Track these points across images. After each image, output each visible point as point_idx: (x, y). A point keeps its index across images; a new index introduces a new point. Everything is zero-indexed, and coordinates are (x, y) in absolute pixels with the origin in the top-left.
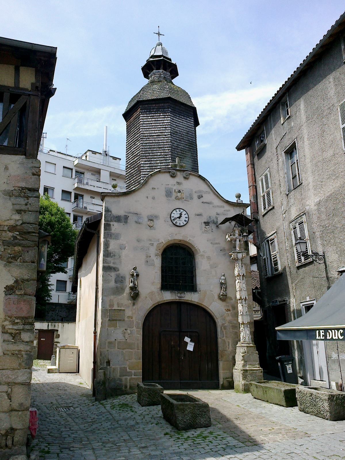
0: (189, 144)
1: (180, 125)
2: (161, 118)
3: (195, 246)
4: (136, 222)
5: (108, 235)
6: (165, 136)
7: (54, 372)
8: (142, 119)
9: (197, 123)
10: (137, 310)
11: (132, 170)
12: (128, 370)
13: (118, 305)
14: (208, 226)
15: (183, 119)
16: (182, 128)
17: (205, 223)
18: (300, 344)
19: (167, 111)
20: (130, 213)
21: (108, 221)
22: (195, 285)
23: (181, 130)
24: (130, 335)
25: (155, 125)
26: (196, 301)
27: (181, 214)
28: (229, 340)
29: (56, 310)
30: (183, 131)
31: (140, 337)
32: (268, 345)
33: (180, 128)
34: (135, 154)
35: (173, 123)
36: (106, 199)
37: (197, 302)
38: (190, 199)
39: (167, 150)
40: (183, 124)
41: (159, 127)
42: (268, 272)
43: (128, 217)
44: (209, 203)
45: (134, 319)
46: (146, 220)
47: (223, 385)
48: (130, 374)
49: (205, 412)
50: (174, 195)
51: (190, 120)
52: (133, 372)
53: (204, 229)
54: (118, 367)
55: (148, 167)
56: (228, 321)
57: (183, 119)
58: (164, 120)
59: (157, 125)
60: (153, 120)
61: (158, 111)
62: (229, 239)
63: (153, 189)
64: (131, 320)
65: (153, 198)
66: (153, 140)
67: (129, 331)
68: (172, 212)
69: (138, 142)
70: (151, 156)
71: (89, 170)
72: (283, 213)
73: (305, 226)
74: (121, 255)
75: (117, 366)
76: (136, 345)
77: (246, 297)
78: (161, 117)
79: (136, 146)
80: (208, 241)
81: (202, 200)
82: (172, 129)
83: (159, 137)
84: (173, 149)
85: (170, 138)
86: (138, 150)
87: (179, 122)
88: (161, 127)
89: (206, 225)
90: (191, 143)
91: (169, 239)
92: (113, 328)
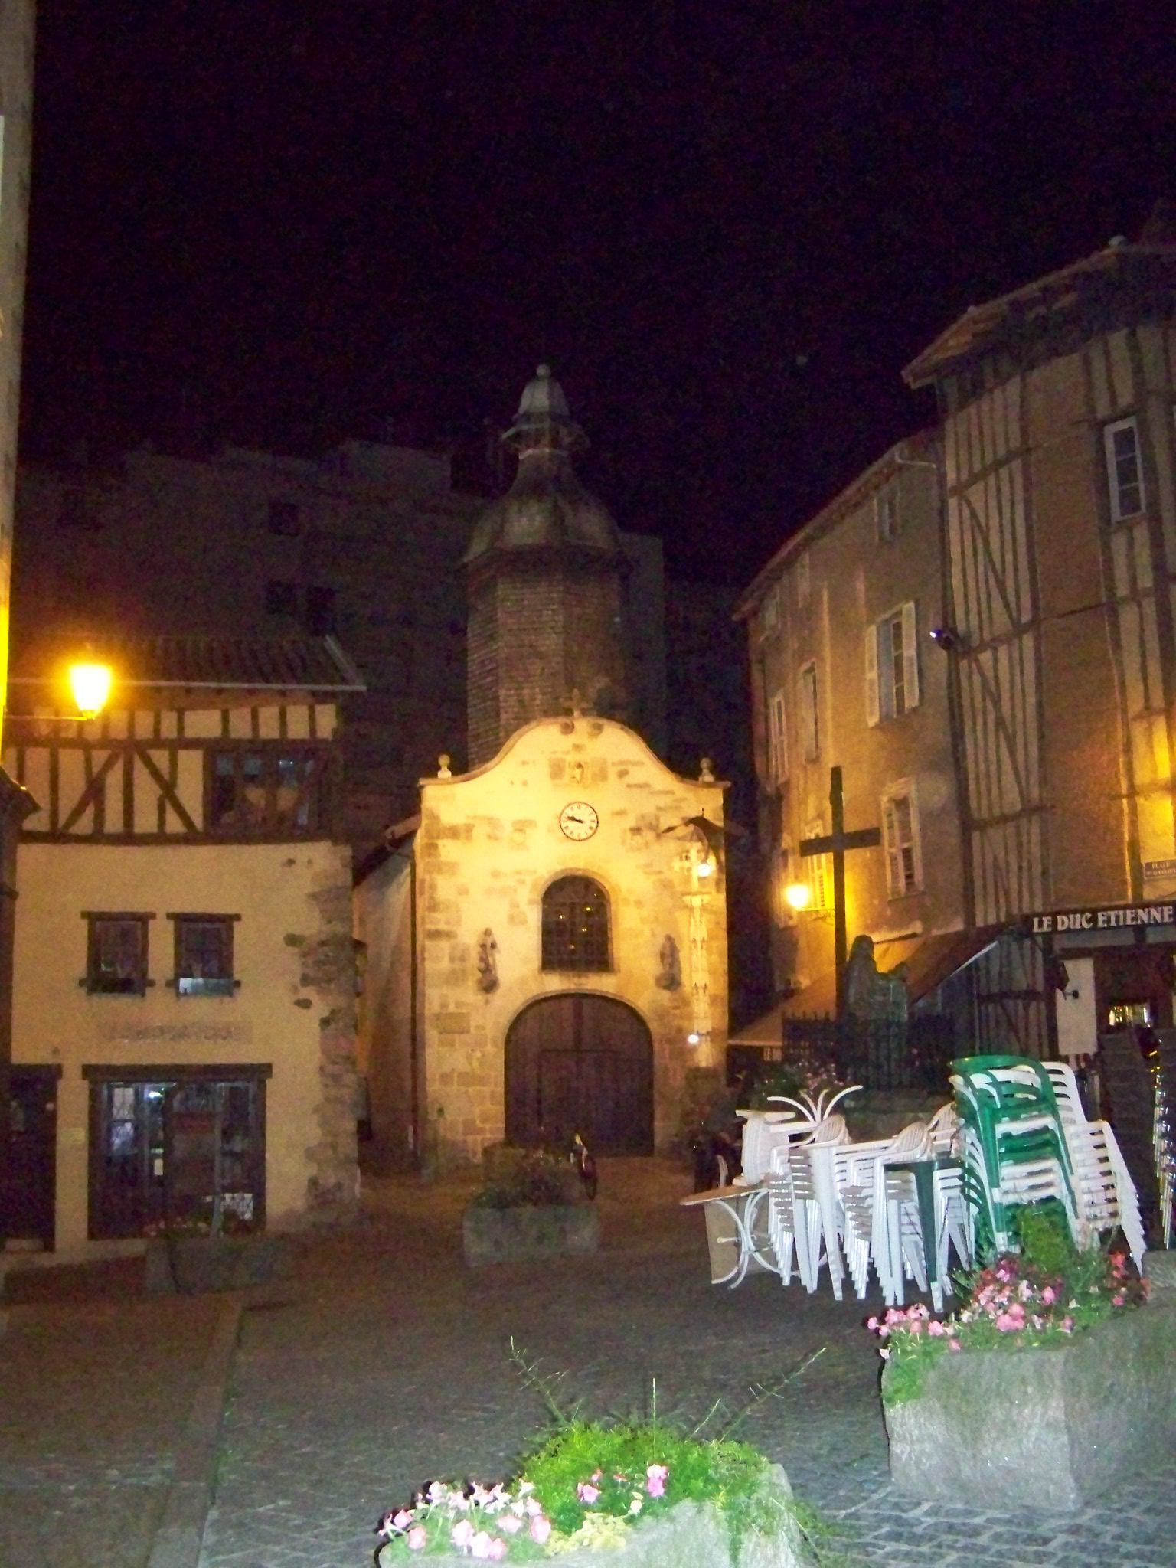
20: (475, 817)
46: (509, 828)
48: (481, 1131)
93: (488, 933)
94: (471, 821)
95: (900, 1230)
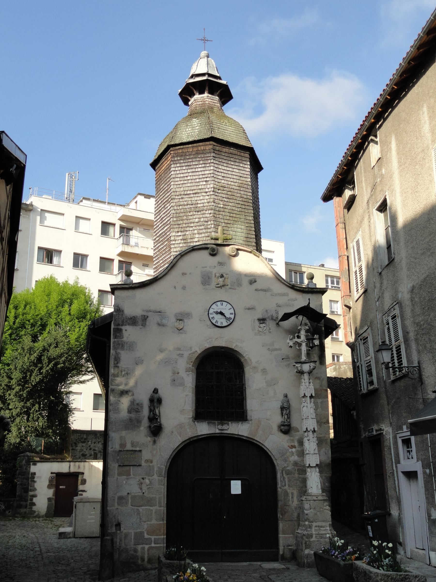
0: (242, 203)
1: (228, 176)
3: (244, 355)
4: (159, 324)
5: (119, 344)
7: (68, 536)
8: (174, 171)
10: (158, 450)
11: (160, 245)
12: (146, 536)
13: (133, 444)
14: (264, 325)
15: (233, 167)
17: (259, 320)
18: (398, 494)
20: (150, 311)
22: (245, 411)
24: (149, 486)
27: (217, 313)
28: (293, 491)
29: (88, 442)
30: (232, 183)
31: (163, 489)
32: (365, 493)
33: (229, 179)
34: (164, 222)
37: (246, 437)
38: (238, 286)
40: (234, 173)
42: (362, 387)
43: (148, 317)
45: (154, 463)
46: (172, 319)
47: (283, 555)
48: (149, 541)
50: (214, 281)
51: (244, 166)
52: (153, 539)
53: (257, 328)
54: (132, 532)
56: (292, 462)
60: (189, 171)
63: (184, 274)
64: (151, 464)
65: (184, 288)
67: (147, 481)
69: (169, 204)
70: (186, 224)
72: (376, 300)
73: (399, 321)
75: (130, 531)
76: (157, 500)
79: (166, 210)
80: (263, 346)
81: (255, 286)
82: (217, 183)
83: (197, 195)
84: (217, 212)
85: (212, 197)
86: (168, 215)
87: (227, 172)
89: (261, 323)
90: (245, 200)
91: (205, 347)
92: (126, 477)
93: (156, 391)
94: (145, 314)
95: (223, 232)
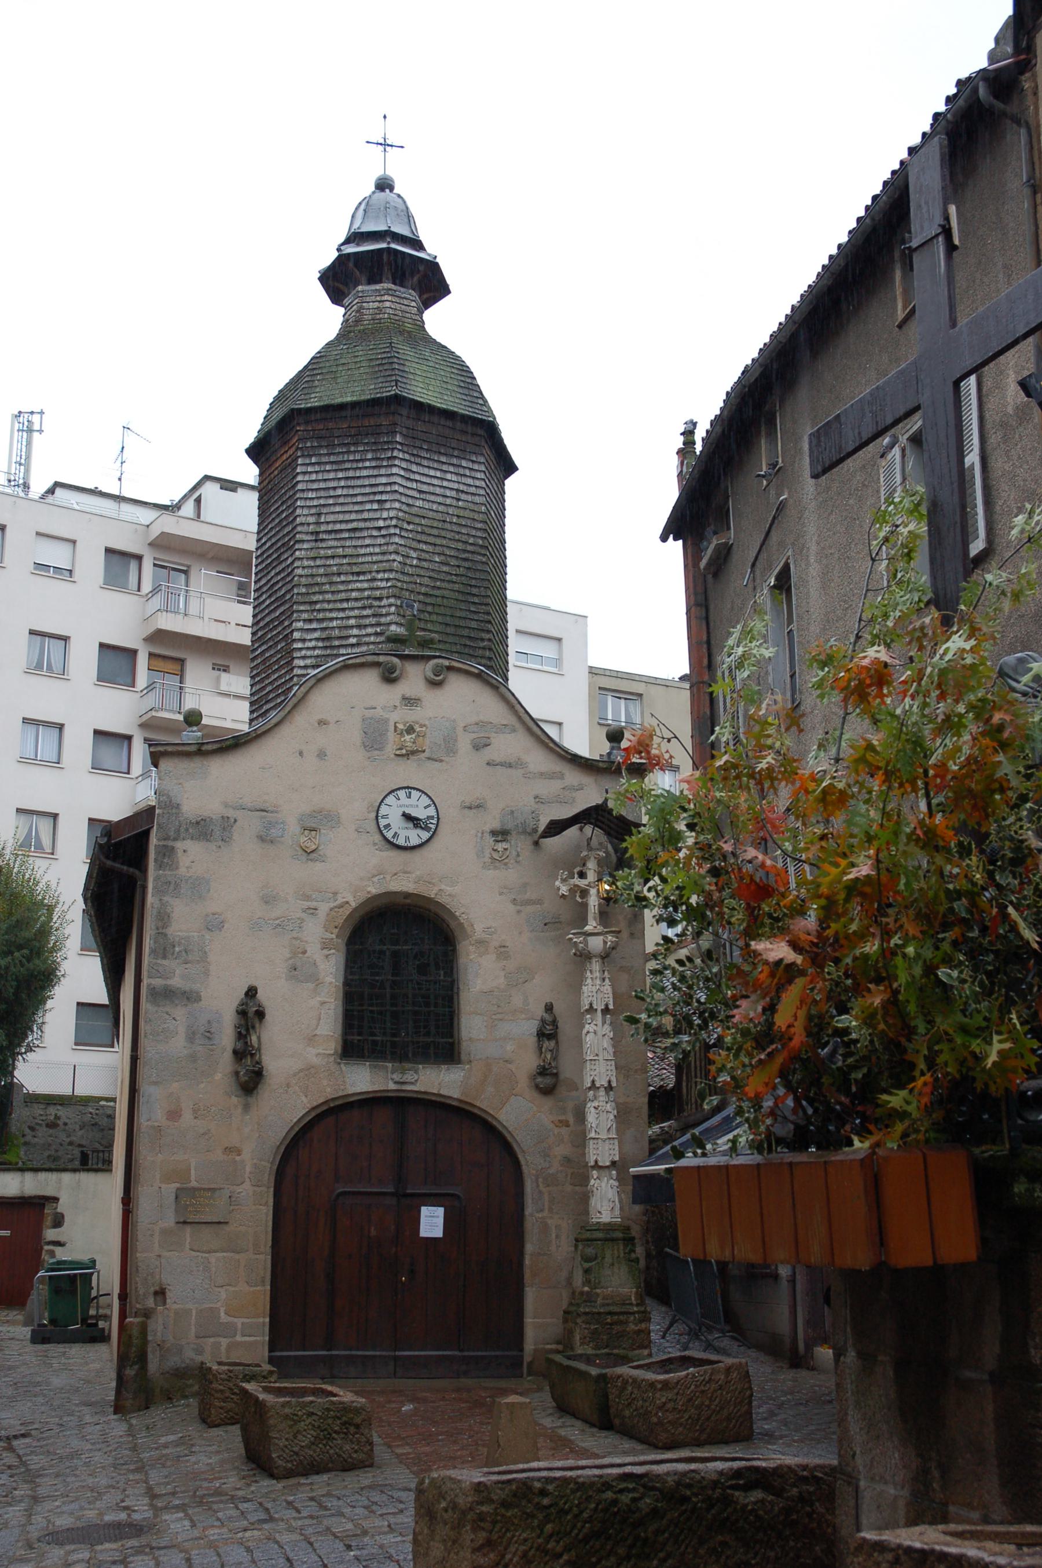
2: (366, 468)
6: (375, 533)
9: (507, 466)
12: (224, 1318)
14: (505, 845)
16: (440, 499)
17: (494, 833)
19: (388, 442)
21: (167, 838)
23: (435, 507)
25: (345, 491)
26: (455, 1096)
31: (266, 1213)
33: (432, 498)
35: (409, 484)
36: (164, 764)
37: (460, 1101)
39: (381, 580)
40: (445, 484)
41: (359, 499)
43: (235, 821)
44: (510, 766)
45: (246, 1155)
48: (228, 1330)
49: (357, 1426)
51: (470, 465)
52: (239, 1326)
55: (317, 639)
57: (445, 467)
58: (376, 476)
59: (351, 492)
60: (340, 475)
61: (356, 437)
62: (564, 890)
64: (238, 1158)
65: (322, 755)
66: (337, 547)
68: (382, 801)
71: (210, 555)
74: (207, 949)
77: (609, 1082)
78: (367, 464)
81: (488, 754)
87: (428, 480)
88: (365, 499)
